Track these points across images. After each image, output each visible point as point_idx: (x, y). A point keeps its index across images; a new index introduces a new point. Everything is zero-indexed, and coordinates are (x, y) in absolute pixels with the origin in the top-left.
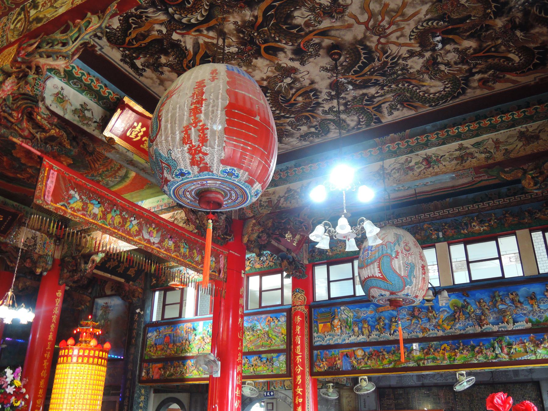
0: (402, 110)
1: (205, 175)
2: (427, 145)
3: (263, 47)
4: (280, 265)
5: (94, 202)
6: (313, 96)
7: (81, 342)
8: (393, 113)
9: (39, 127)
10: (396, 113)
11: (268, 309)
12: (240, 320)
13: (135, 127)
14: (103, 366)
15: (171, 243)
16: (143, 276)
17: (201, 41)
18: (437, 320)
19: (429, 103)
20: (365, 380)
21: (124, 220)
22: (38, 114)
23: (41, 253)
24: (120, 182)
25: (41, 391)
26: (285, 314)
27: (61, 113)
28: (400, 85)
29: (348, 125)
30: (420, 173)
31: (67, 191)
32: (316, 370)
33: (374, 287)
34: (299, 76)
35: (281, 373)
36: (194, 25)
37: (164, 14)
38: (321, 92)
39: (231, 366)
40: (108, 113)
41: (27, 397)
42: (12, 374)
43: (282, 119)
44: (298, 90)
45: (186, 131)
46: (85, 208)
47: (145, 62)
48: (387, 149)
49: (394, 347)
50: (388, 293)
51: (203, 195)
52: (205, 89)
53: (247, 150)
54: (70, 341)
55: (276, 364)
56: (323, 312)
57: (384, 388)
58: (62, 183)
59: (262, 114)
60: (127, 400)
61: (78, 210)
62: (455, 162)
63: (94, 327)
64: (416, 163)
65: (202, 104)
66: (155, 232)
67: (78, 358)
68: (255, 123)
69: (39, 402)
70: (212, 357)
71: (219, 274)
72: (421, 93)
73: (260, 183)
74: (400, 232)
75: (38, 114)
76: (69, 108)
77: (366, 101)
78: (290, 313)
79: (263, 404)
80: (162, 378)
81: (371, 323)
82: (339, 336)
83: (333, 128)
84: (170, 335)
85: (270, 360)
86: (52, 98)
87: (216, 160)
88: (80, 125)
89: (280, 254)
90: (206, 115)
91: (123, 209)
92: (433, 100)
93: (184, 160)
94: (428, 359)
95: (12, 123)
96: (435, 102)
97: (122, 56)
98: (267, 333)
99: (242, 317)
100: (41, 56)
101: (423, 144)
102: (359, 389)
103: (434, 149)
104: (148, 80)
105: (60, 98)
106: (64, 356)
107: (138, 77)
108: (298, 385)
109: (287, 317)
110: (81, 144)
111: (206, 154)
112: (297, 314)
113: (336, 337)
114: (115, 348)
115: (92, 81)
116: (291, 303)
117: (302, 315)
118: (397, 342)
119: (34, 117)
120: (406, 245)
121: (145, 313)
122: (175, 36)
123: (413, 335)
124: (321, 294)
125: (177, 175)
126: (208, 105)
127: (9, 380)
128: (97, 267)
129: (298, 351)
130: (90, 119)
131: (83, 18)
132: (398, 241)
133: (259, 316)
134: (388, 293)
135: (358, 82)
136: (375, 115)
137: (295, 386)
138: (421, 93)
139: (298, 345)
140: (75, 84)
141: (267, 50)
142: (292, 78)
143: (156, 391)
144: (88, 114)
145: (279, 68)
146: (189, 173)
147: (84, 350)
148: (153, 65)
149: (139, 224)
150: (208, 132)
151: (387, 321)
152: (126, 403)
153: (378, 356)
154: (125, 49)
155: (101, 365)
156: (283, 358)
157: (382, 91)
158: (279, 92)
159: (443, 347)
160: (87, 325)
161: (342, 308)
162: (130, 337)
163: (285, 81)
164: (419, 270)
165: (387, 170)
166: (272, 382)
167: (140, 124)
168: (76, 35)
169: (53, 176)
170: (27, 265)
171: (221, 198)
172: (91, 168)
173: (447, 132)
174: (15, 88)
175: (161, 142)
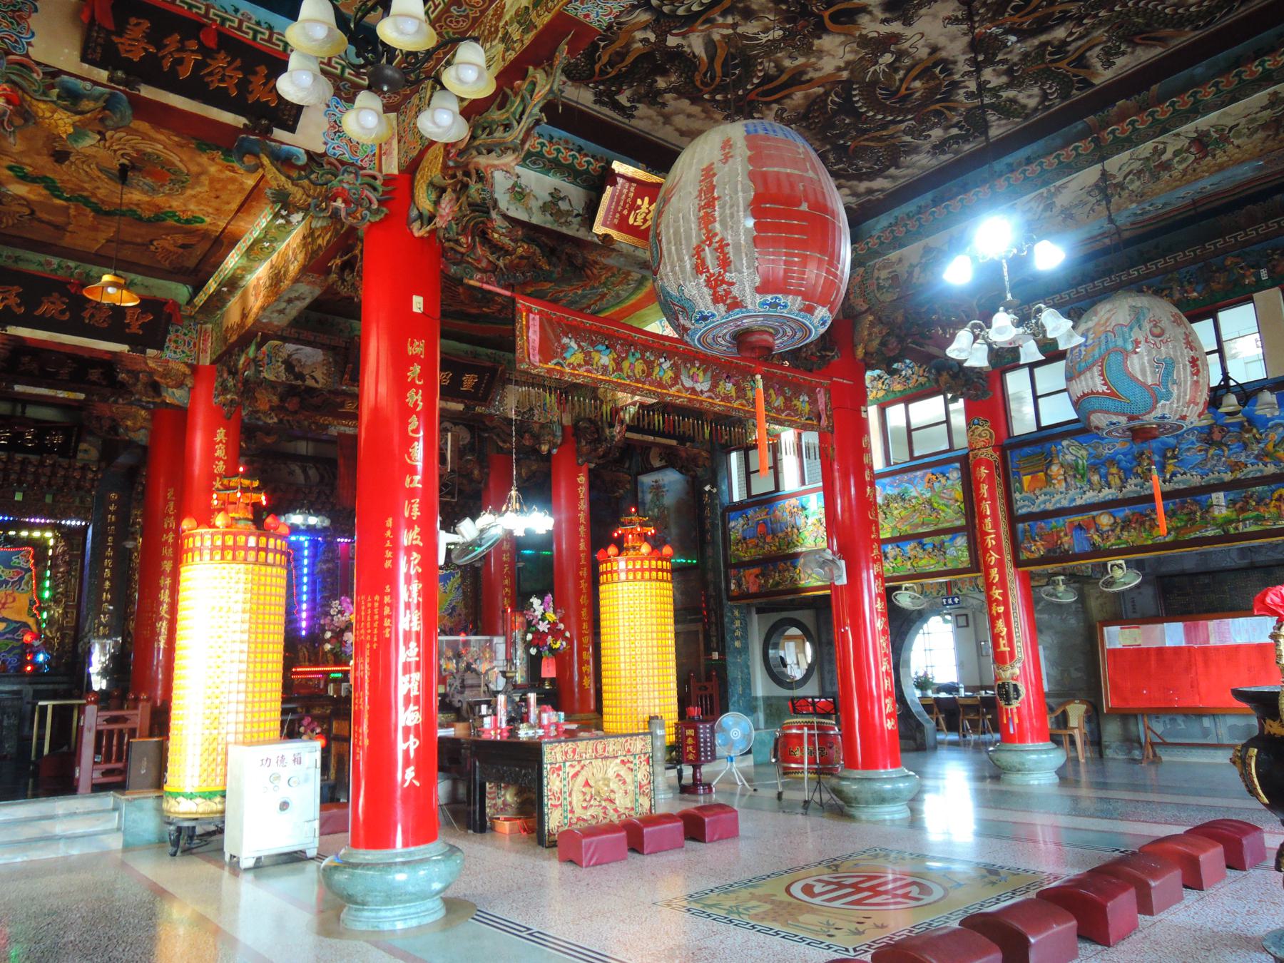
0: (1132, 53)
1: (737, 314)
2: (1196, 111)
3: (826, 15)
4: (937, 381)
6: (941, 72)
7: (628, 549)
8: (1114, 63)
9: (496, 248)
10: (1120, 61)
11: (926, 460)
12: (868, 489)
13: (639, 207)
14: (667, 581)
15: (729, 386)
16: (702, 439)
17: (716, 37)
18: (1262, 445)
19: (1192, 23)
20: (1120, 567)
21: (650, 365)
22: (494, 230)
23: (542, 420)
24: (637, 289)
25: (585, 626)
26: (958, 465)
27: (522, 216)
28: (1117, 8)
29: (1024, 107)
30: (1185, 172)
31: (559, 341)
32: (1024, 556)
33: (1095, 411)
34: (906, 45)
35: (960, 566)
36: (699, 14)
37: (646, 10)
38: (955, 62)
39: (863, 564)
40: (594, 194)
41: (568, 634)
43: (891, 127)
44: (909, 70)
45: (698, 253)
46: (588, 361)
47: (633, 95)
48: (1111, 137)
49: (1174, 504)
50: (1123, 419)
51: (741, 338)
52: (715, 179)
53: (794, 264)
54: (612, 550)
55: (951, 552)
56: (1028, 455)
57: (1172, 576)
58: (549, 330)
59: (811, 197)
60: (714, 628)
61: (580, 366)
62: (1260, 135)
63: (641, 525)
64: (1176, 154)
65: (714, 207)
66: (701, 374)
68: (802, 216)
69: (585, 640)
70: (829, 555)
71: (819, 421)
72: (1167, 11)
73: (824, 306)
74: (1142, 301)
76: (535, 205)
77: (1051, 54)
78: (967, 464)
79: (948, 617)
80: (763, 590)
81: (1123, 464)
82: (1062, 494)
83: (994, 118)
84: (765, 522)
85: (940, 548)
86: (507, 196)
87: (747, 288)
88: (555, 227)
89: (933, 362)
90: (723, 223)
91: (646, 347)
92: (1199, 15)
93: (703, 298)
94: (1244, 520)
95: (463, 254)
96: (1202, 18)
97: (595, 94)
98: (929, 502)
99: (872, 485)
100: (480, 153)
101: (1189, 111)
102: (1111, 583)
103: (1213, 116)
104: (644, 120)
105: (519, 193)
106: (607, 573)
107: (627, 121)
108: (993, 584)
109: (961, 470)
110: (564, 257)
111: (732, 284)
112: (979, 463)
113: (1057, 497)
114: (682, 549)
115: (558, 151)
116: (966, 445)
117: (989, 465)
118: (1150, 498)
119: (489, 236)
120: (1155, 326)
122: (672, 41)
123: (1212, 478)
124: (1023, 421)
125: (697, 321)
126: (723, 207)
127: (538, 613)
128: (630, 428)
129: (988, 527)
130: (568, 213)
131: (524, 76)
132: (1138, 320)
133: (911, 475)
134: (1123, 419)
135: (1025, 26)
136: (1075, 75)
137: (989, 585)
138: (1167, 11)
139: (986, 517)
140: (534, 163)
141: (835, 18)
142: (892, 53)
143: (760, 611)
144: (563, 206)
145: (864, 41)
146: (713, 315)
147: (634, 560)
148: (647, 95)
149: (674, 366)
150: (730, 249)
151: (1156, 458)
152: (713, 631)
153: (1142, 524)
154: (597, 83)
155: (662, 580)
156: (961, 541)
157: (1081, 29)
158: (874, 82)
159: (1276, 495)
160: (631, 523)
161: (1065, 443)
162: (703, 532)
163: (881, 61)
164: (1184, 369)
165: (1114, 177)
166: (955, 582)
167: (647, 199)
168: (520, 109)
169: (535, 321)
170: (527, 443)
171: (770, 339)
172: (588, 277)
173: (1238, 75)
174: (456, 208)
175: (666, 275)
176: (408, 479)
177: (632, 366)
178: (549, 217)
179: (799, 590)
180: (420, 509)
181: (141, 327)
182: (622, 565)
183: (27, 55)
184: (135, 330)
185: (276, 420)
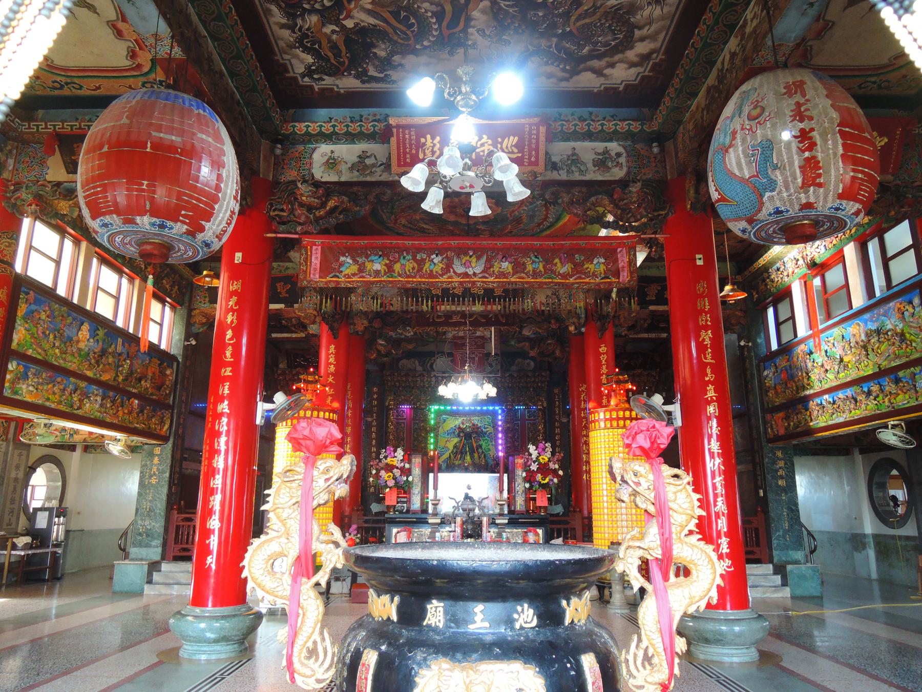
5: (373, 258)
13: (424, 144)
22: (302, 195)
31: (338, 260)
61: (354, 275)
75: (302, 195)
88: (362, 179)
98: (902, 335)
121: (755, 343)
167: (429, 137)
170: (554, 327)
176: (223, 370)
177: (403, 266)
178: (356, 173)
179: (811, 432)
180: (229, 389)
181: (287, 292)
182: (602, 416)
183: (45, 180)
184: (284, 295)
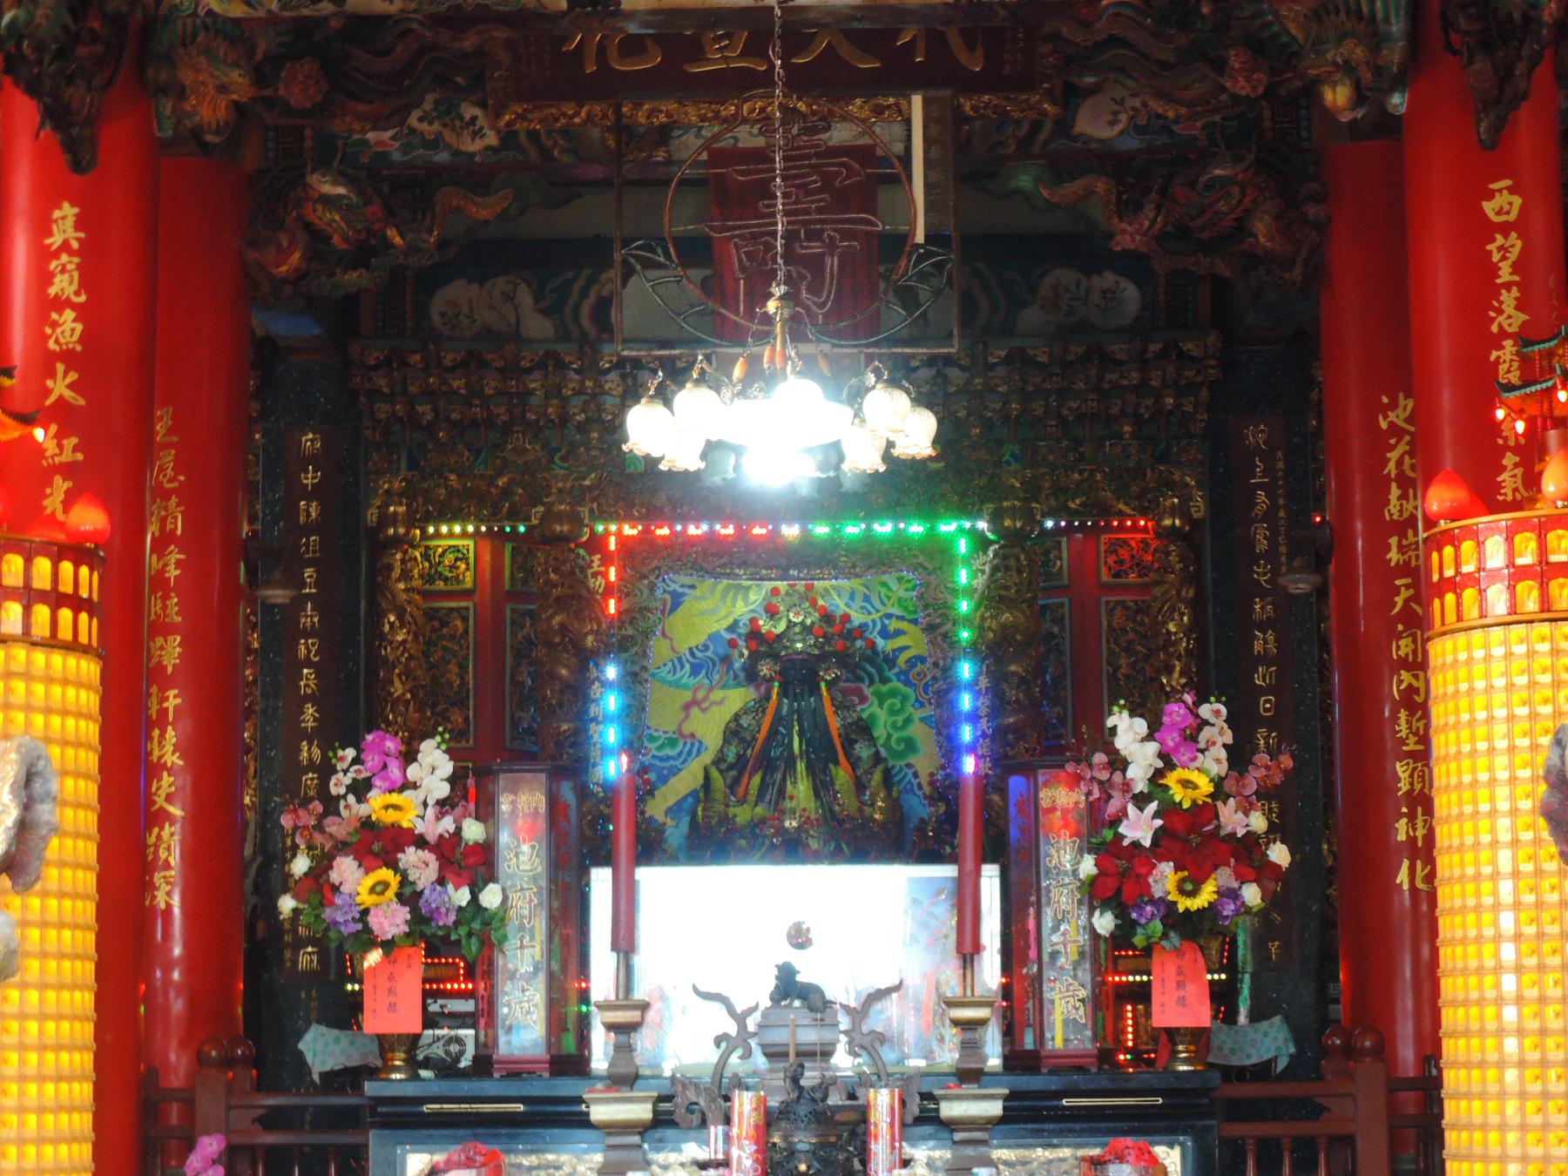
42: (1150, 737)
67: (1511, 589)
155: (52, 643)
185: (491, 139)
